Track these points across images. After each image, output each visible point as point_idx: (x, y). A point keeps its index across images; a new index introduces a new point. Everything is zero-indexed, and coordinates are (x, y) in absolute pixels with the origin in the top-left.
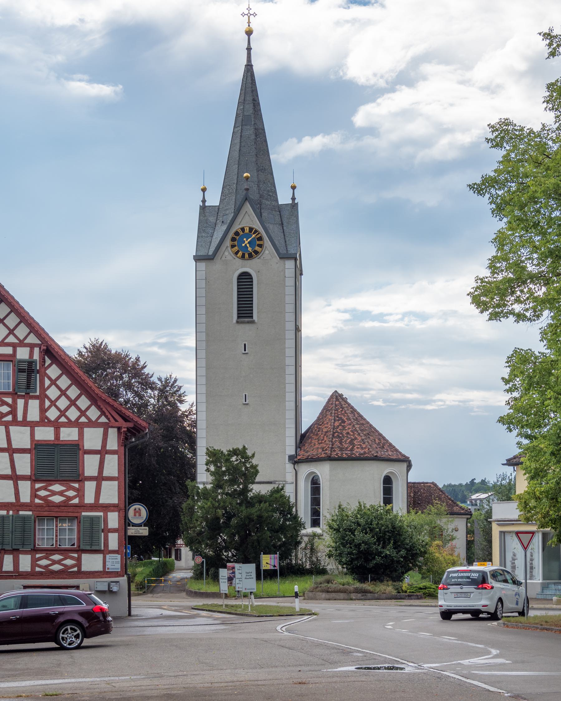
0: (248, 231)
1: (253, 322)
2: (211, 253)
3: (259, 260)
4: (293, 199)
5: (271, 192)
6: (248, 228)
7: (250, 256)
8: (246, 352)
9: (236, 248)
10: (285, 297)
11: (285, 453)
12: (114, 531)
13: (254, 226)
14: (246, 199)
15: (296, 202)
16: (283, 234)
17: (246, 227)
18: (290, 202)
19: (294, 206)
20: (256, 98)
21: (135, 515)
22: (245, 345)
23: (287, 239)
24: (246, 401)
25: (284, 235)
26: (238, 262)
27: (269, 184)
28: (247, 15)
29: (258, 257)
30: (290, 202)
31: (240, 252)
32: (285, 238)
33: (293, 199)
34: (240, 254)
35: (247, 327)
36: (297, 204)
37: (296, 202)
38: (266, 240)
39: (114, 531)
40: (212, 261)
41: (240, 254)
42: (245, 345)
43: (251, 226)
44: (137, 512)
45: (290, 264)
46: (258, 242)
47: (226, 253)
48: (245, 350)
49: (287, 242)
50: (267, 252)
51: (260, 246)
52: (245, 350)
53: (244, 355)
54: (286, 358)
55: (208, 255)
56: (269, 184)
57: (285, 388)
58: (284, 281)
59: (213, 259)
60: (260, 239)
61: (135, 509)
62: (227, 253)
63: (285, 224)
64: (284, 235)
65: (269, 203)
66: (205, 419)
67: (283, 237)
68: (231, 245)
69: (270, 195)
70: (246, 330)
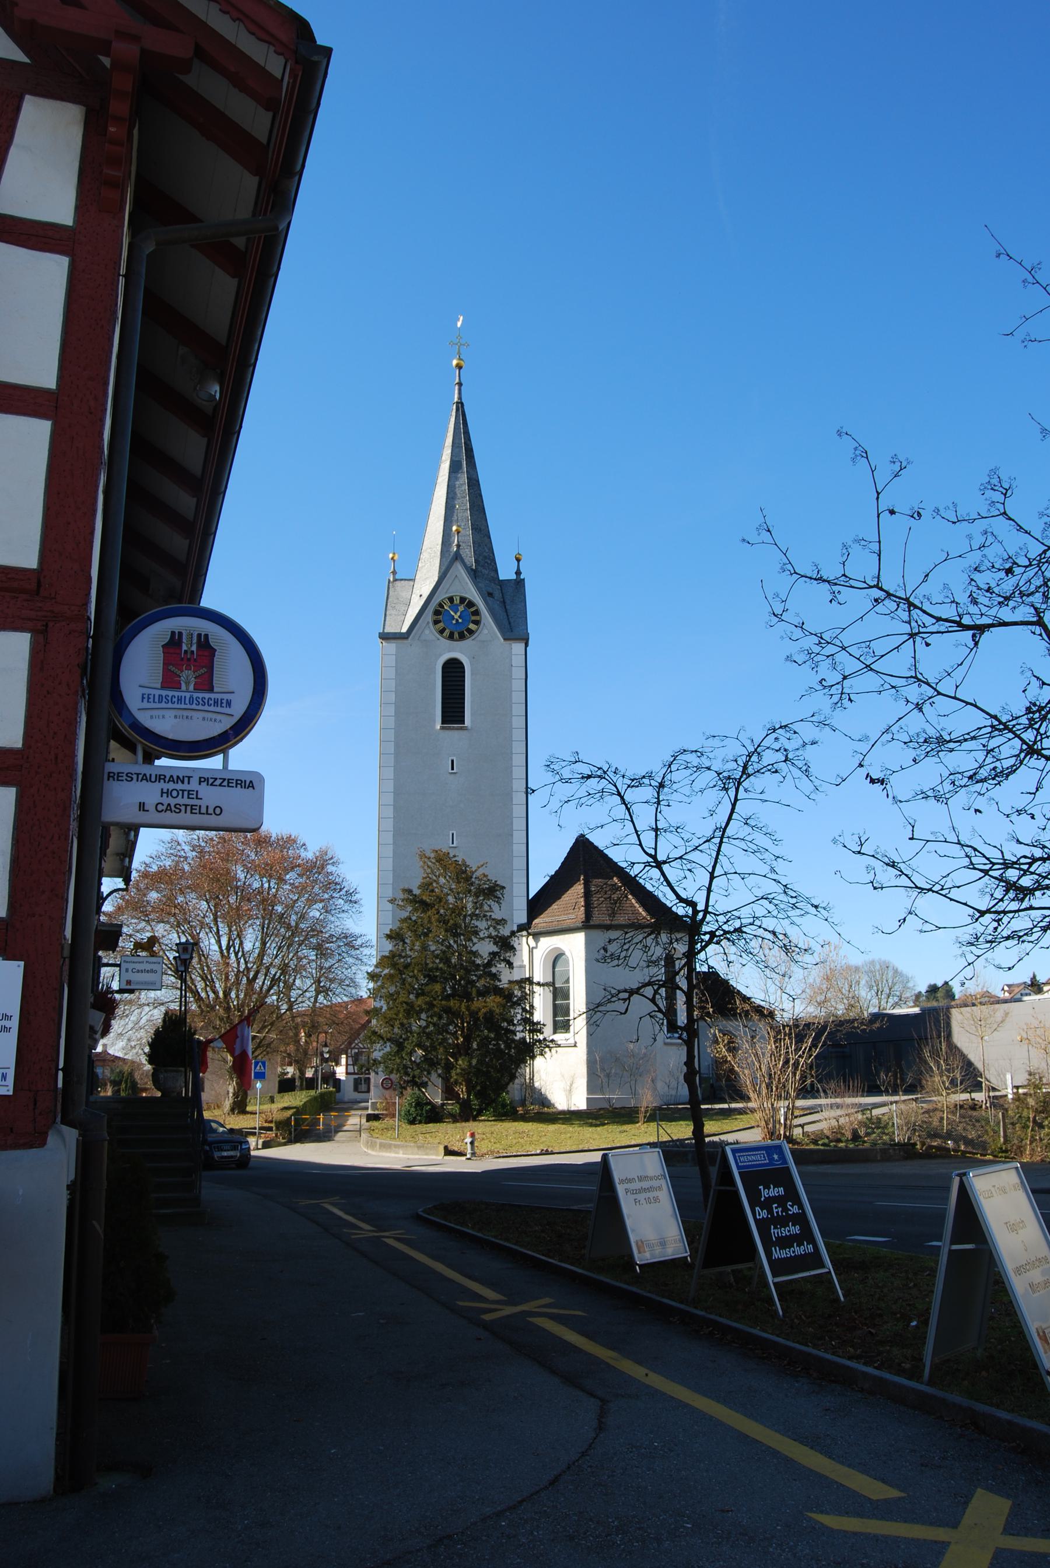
0: (458, 602)
1: (465, 729)
2: (404, 630)
3: (474, 642)
4: (518, 573)
5: (489, 559)
6: (458, 598)
7: (462, 637)
8: (455, 771)
9: (441, 625)
10: (511, 693)
11: (513, 921)
12: (698, 1132)
13: (466, 596)
14: (456, 559)
15: (522, 577)
16: (505, 614)
17: (456, 596)
18: (514, 577)
19: (519, 584)
20: (468, 442)
21: (170, 681)
22: (452, 761)
23: (512, 620)
24: (453, 843)
25: (508, 616)
26: (445, 642)
27: (485, 548)
28: (457, 344)
29: (473, 637)
30: (514, 577)
31: (447, 631)
32: (508, 619)
33: (518, 573)
34: (447, 633)
35: (455, 734)
36: (524, 580)
37: (522, 577)
38: (484, 614)
39: (698, 1132)
40: (405, 641)
41: (447, 633)
42: (452, 761)
43: (464, 595)
44: (189, 661)
45: (518, 647)
46: (473, 618)
47: (427, 632)
48: (453, 769)
49: (512, 624)
50: (485, 631)
51: (477, 623)
52: (453, 769)
53: (453, 775)
54: (514, 781)
55: (401, 633)
56: (485, 548)
57: (512, 823)
58: (511, 671)
59: (407, 638)
60: (477, 613)
61: (174, 642)
62: (430, 632)
63: (508, 602)
64: (508, 616)
65: (487, 572)
66: (391, 869)
67: (505, 617)
68: (434, 621)
69: (487, 562)
70: (454, 737)
